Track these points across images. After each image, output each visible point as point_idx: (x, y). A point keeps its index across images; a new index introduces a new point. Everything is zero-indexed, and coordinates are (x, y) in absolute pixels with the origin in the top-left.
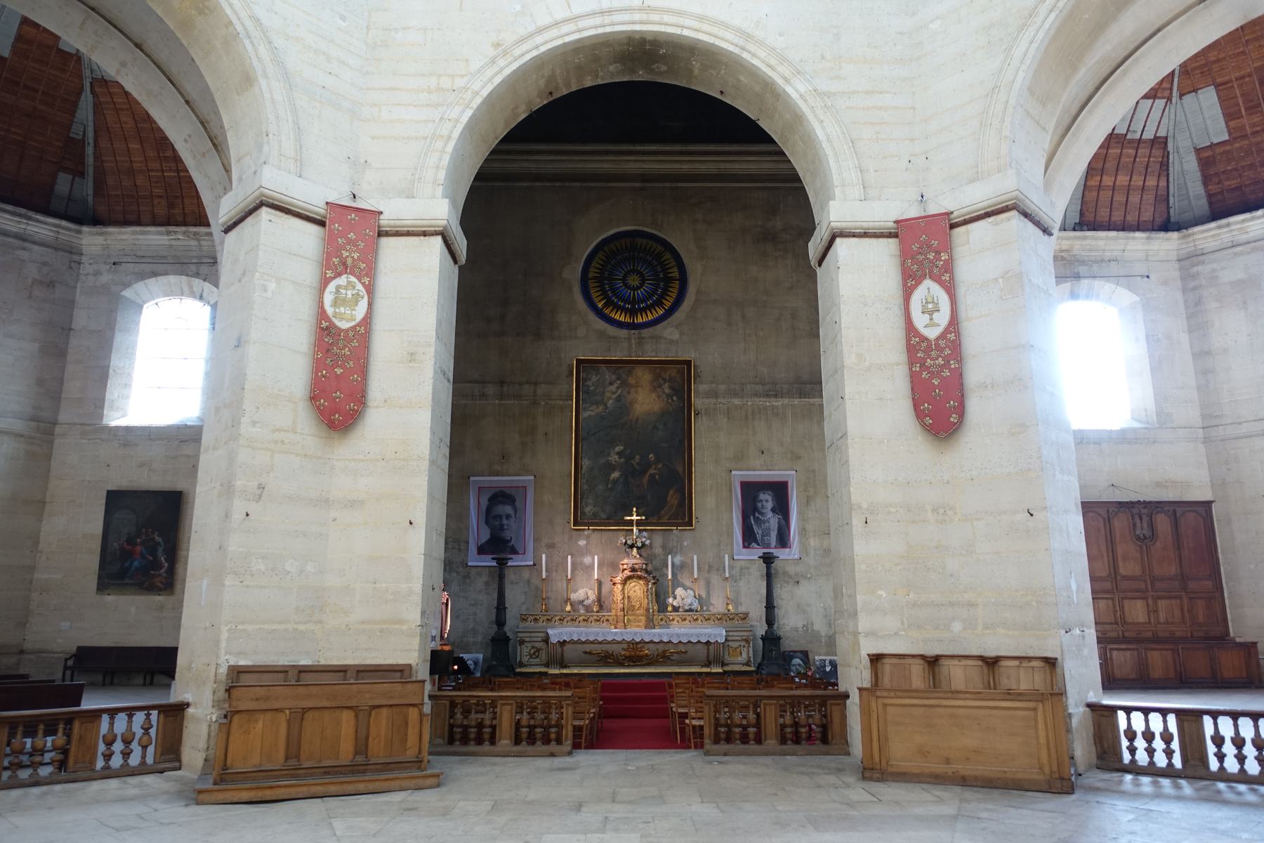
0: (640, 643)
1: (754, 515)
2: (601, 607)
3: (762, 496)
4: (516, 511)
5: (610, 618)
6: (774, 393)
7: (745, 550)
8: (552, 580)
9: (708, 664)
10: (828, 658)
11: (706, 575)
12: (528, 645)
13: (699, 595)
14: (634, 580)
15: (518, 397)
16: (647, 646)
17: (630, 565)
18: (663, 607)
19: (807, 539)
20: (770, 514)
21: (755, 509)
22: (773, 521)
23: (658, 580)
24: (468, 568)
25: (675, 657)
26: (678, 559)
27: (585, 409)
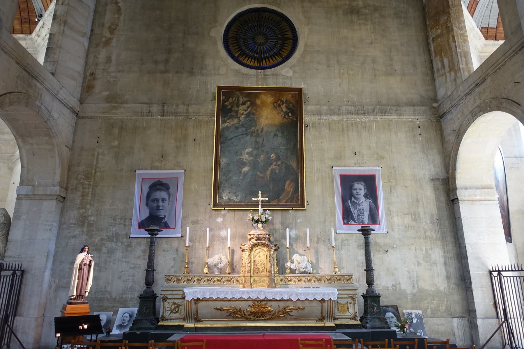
0: (263, 300)
1: (351, 199)
2: (233, 270)
3: (357, 186)
4: (169, 196)
5: (239, 279)
6: (363, 112)
7: (345, 226)
8: (195, 249)
9: (322, 319)
10: (414, 312)
11: (315, 245)
12: (170, 301)
13: (311, 261)
14: (259, 247)
15: (175, 114)
16: (269, 303)
17: (255, 235)
18: (282, 270)
19: (392, 218)
20: (363, 199)
21: (351, 195)
22: (365, 204)
23: (279, 248)
24: (131, 239)
25: (294, 313)
26: (294, 233)
27: (225, 122)
